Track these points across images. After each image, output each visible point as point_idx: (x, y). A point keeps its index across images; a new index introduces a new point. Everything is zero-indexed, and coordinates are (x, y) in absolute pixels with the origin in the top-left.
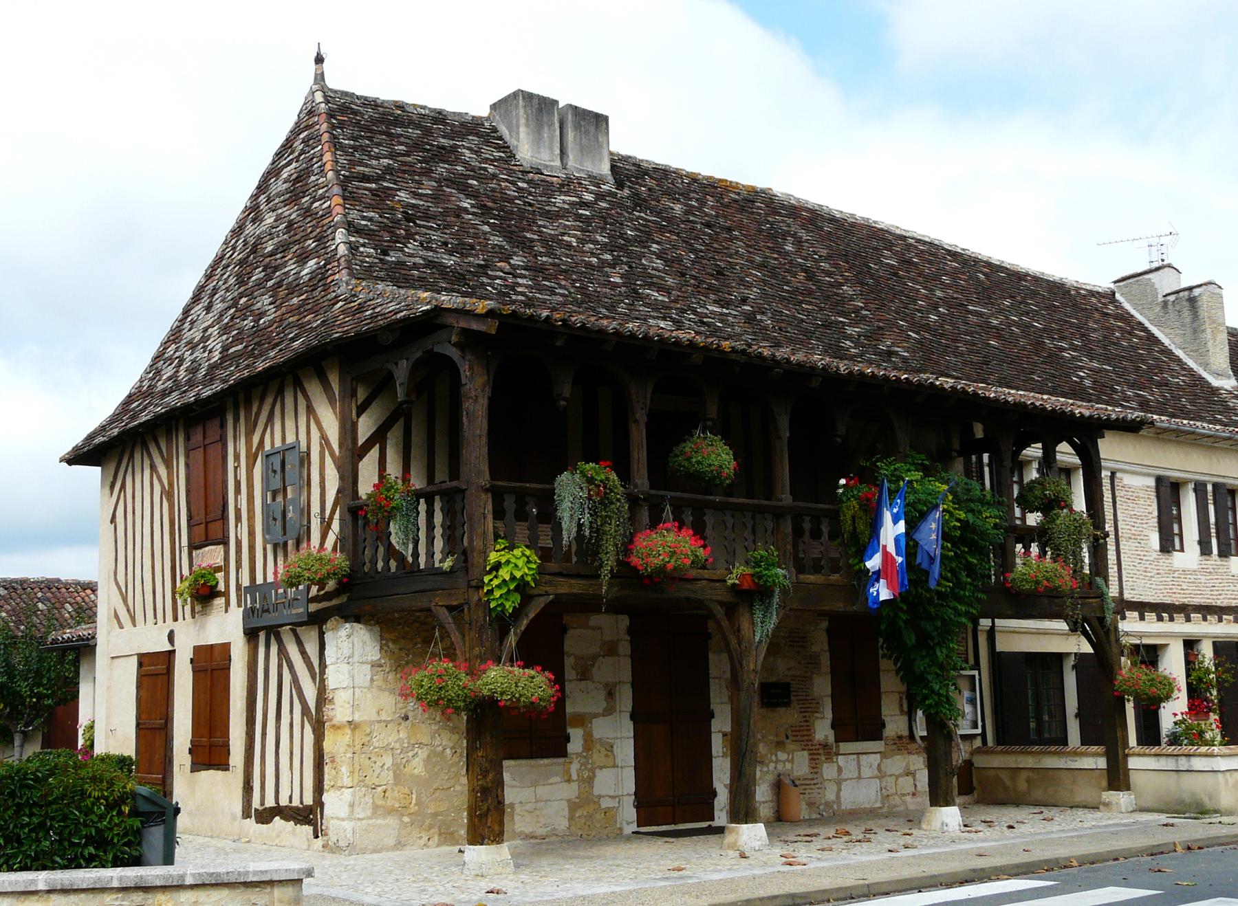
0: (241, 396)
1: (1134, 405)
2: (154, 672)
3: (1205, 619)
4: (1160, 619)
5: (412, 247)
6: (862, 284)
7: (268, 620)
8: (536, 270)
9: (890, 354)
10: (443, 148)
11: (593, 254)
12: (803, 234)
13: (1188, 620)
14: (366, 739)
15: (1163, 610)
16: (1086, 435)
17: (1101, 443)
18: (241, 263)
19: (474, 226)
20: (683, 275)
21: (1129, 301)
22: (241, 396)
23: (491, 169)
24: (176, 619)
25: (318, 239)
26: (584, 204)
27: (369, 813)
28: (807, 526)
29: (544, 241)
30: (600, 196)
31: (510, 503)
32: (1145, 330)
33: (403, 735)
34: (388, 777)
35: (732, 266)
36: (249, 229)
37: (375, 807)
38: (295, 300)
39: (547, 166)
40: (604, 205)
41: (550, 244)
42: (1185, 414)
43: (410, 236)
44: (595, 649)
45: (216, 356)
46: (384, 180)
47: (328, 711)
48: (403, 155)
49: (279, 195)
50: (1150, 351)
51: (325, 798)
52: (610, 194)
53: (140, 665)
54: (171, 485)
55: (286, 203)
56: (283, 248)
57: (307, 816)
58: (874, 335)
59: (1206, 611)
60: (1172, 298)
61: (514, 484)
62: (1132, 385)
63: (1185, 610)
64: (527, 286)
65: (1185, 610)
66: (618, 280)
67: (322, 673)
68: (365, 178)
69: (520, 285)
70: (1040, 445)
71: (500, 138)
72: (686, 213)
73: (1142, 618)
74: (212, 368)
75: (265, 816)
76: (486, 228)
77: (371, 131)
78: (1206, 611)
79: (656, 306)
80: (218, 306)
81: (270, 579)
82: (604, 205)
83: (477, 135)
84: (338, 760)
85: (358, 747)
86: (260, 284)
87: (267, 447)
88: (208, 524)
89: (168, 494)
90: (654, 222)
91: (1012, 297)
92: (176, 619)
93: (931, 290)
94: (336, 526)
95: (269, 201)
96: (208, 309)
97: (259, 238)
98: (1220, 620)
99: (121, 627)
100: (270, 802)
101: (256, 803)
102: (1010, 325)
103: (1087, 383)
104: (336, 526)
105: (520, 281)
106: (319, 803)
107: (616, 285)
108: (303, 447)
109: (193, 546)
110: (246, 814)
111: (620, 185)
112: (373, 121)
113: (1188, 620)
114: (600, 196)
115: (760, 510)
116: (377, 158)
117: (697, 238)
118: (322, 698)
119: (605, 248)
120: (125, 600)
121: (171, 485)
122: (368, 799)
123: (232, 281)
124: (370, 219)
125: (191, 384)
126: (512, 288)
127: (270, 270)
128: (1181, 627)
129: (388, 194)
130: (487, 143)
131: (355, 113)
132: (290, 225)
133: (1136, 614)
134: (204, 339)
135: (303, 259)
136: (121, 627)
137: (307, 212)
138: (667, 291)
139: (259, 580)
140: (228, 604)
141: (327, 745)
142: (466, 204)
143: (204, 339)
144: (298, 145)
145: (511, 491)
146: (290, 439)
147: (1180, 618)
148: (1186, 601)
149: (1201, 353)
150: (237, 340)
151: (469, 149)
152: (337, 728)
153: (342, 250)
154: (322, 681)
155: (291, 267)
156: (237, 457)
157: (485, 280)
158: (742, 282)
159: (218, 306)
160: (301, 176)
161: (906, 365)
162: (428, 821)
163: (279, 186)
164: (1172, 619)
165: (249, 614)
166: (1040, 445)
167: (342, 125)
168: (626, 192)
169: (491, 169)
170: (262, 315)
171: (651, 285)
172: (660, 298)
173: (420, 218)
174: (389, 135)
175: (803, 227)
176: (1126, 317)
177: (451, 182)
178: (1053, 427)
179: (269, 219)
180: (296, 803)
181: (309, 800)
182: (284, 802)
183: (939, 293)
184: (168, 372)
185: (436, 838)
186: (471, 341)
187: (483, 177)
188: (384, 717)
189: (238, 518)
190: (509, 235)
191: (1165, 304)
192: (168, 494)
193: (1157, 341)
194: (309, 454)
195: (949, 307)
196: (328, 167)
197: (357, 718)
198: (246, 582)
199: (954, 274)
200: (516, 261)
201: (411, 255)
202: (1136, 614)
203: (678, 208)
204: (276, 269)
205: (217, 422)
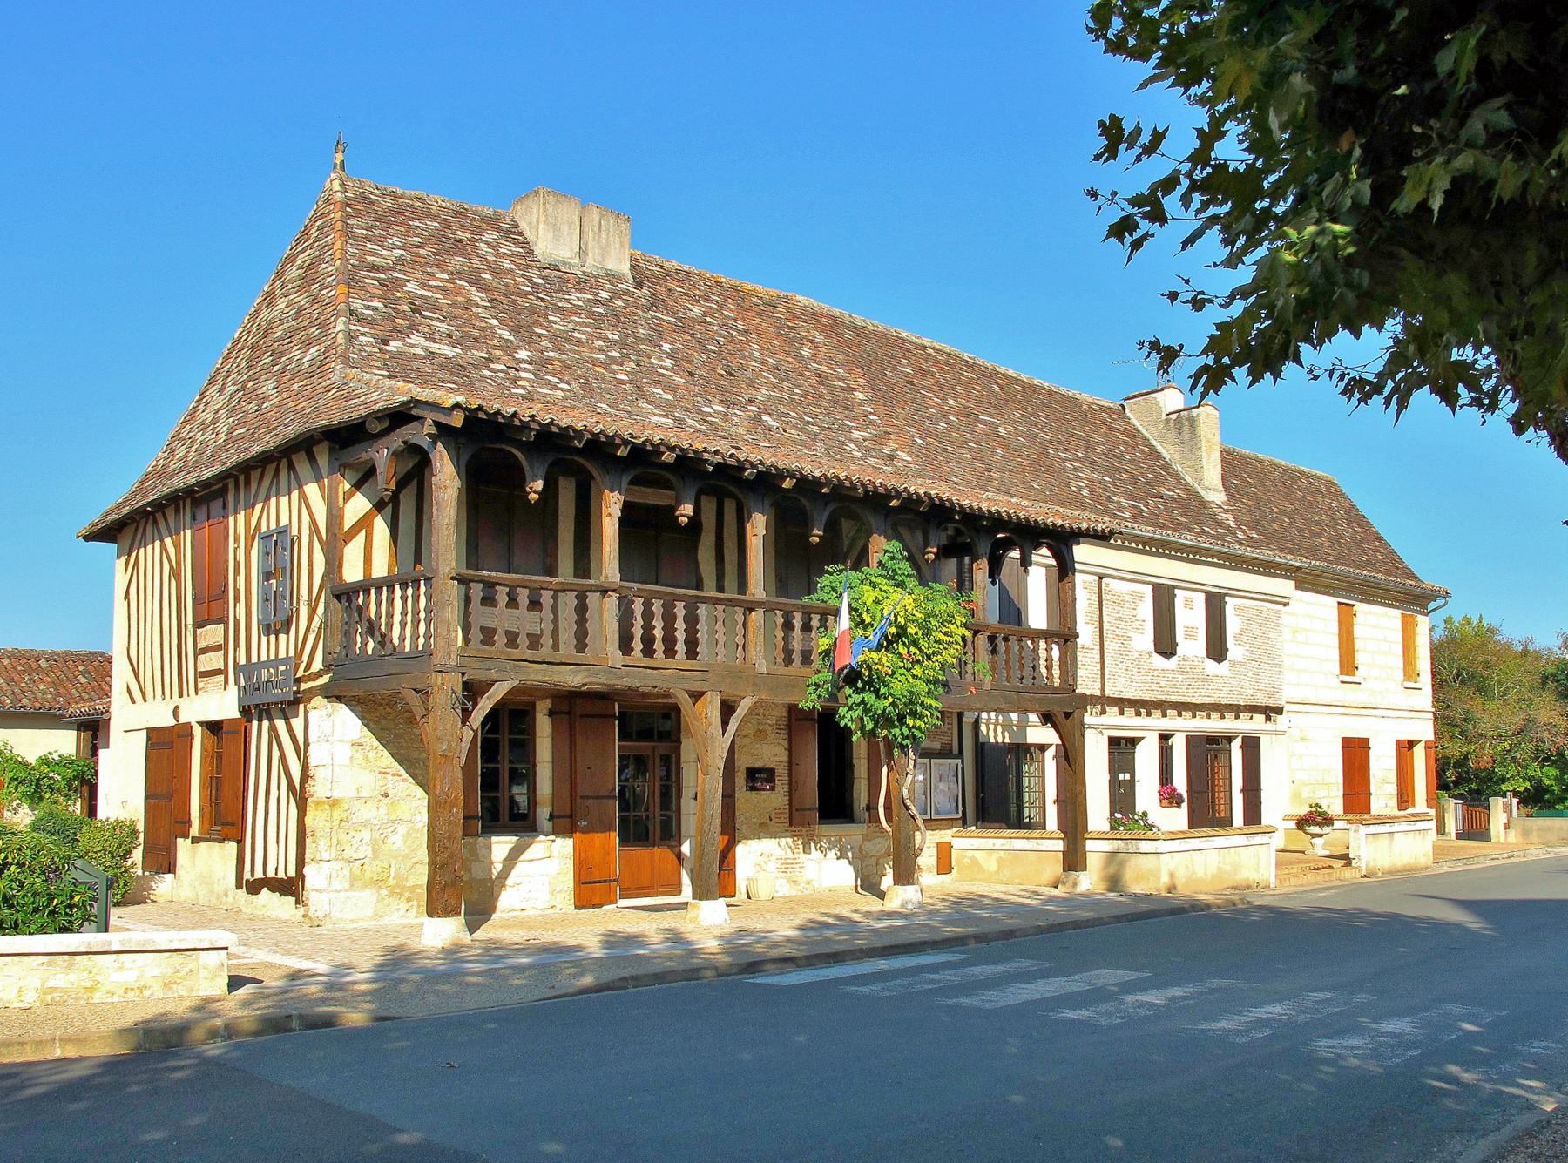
0: (242, 478)
1: (1127, 515)
2: (165, 746)
3: (1180, 715)
4: (1138, 714)
5: (415, 339)
6: (874, 390)
7: (258, 699)
8: (541, 363)
9: (892, 458)
10: (460, 241)
11: (601, 351)
12: (820, 339)
13: (1165, 715)
14: (344, 816)
15: (1141, 706)
16: (1061, 541)
17: (1076, 549)
18: (253, 348)
19: (483, 319)
20: (692, 374)
21: (1137, 418)
22: (242, 478)
23: (507, 264)
24: (181, 695)
25: (321, 327)
26: (599, 302)
27: (347, 885)
28: (797, 623)
29: (552, 336)
30: (617, 294)
31: (477, 591)
32: (1150, 445)
33: (383, 811)
34: (365, 851)
35: (743, 368)
36: (264, 314)
37: (353, 880)
38: (295, 386)
39: (565, 263)
40: (620, 303)
41: (559, 341)
42: (1177, 527)
43: (413, 327)
44: (1337, 824)
45: (223, 437)
46: (394, 270)
47: (309, 789)
48: (416, 246)
49: (290, 281)
50: (1151, 465)
51: (306, 871)
52: (627, 292)
53: (149, 739)
54: (178, 563)
55: (299, 289)
56: (291, 333)
57: (290, 887)
58: (881, 439)
59: (1181, 707)
60: (1174, 417)
61: (527, 577)
62: (1129, 497)
63: (1163, 707)
64: (528, 380)
65: (1163, 707)
66: (625, 377)
67: (306, 751)
68: (375, 268)
69: (521, 378)
70: (1044, 551)
71: (520, 234)
72: (705, 314)
73: (1121, 713)
74: (219, 449)
75: (254, 887)
76: (495, 322)
77: (387, 222)
78: (1181, 707)
79: (657, 403)
80: (231, 389)
81: (264, 658)
82: (620, 303)
83: (499, 230)
84: (318, 834)
85: (336, 823)
86: (266, 369)
87: (264, 529)
88: (210, 604)
89: (176, 573)
90: (669, 322)
91: (1024, 409)
92: (181, 695)
93: (944, 399)
94: (321, 609)
95: (283, 287)
96: (221, 391)
97: (271, 323)
98: (1222, 717)
99: (133, 702)
100: (259, 874)
101: (247, 875)
102: (1016, 435)
103: (1085, 492)
104: (321, 609)
105: (523, 374)
106: (300, 875)
107: (623, 382)
108: (295, 532)
109: (199, 624)
110: (239, 886)
111: (639, 285)
112: (390, 211)
113: (1165, 715)
114: (617, 294)
115: (731, 603)
116: (391, 249)
117: (711, 341)
118: (305, 776)
119: (612, 345)
120: (136, 675)
121: (178, 563)
122: (346, 872)
123: (243, 364)
124: (375, 309)
125: (196, 465)
126: (515, 380)
127: (277, 355)
128: (1158, 722)
129: (398, 284)
130: (507, 238)
131: (372, 203)
132: (299, 311)
133: (1116, 709)
134: (215, 421)
135: (307, 344)
136: (133, 702)
137: (315, 299)
138: (672, 389)
139: (254, 659)
140: (226, 682)
141: (308, 820)
142: (477, 295)
143: (215, 421)
144: (314, 233)
145: (659, 596)
146: (284, 522)
147: (1156, 713)
148: (1163, 698)
149: (1197, 468)
150: (241, 423)
151: (487, 243)
152: (317, 803)
153: (341, 339)
154: (306, 757)
155: (295, 352)
156: (237, 540)
157: (486, 372)
158: (752, 384)
159: (231, 389)
160: (311, 267)
161: (905, 472)
162: (407, 894)
163: (293, 272)
164: (1149, 714)
165: (243, 691)
166: (1044, 551)
167: (357, 214)
168: (645, 290)
169: (507, 264)
170: (265, 399)
171: (657, 383)
172: (665, 396)
173: (427, 309)
174: (409, 228)
175: (822, 333)
176: (1133, 433)
177: (461, 274)
178: (1029, 535)
179: (282, 304)
180: (281, 875)
181: (292, 873)
182: (271, 874)
183: (951, 402)
184: (181, 452)
185: (414, 910)
186: (444, 431)
187: (496, 271)
188: (364, 794)
189: (237, 599)
190: (515, 330)
191: (1168, 420)
192: (176, 573)
193: (1158, 456)
194: (299, 538)
195: (959, 414)
196: (338, 255)
197: (336, 795)
198: (242, 661)
199: (968, 386)
200: (523, 354)
201: (413, 346)
202: (1116, 709)
203: (697, 311)
204: (282, 354)
205: (220, 502)
